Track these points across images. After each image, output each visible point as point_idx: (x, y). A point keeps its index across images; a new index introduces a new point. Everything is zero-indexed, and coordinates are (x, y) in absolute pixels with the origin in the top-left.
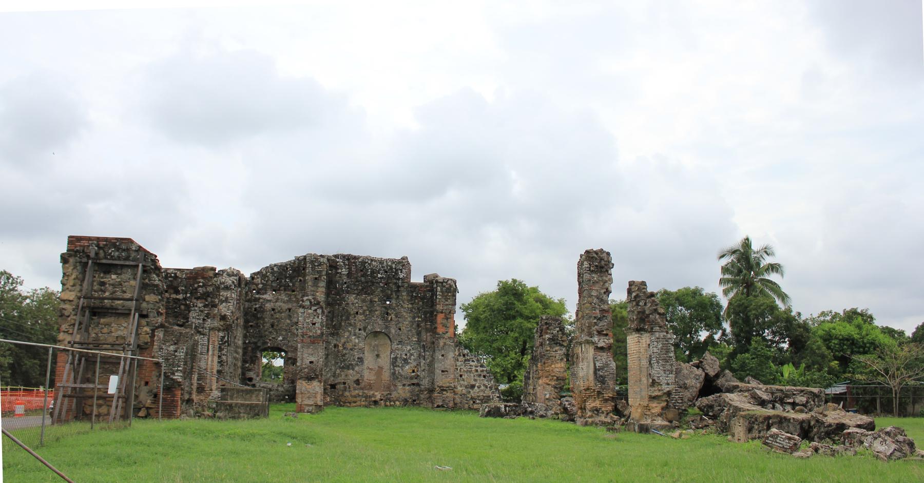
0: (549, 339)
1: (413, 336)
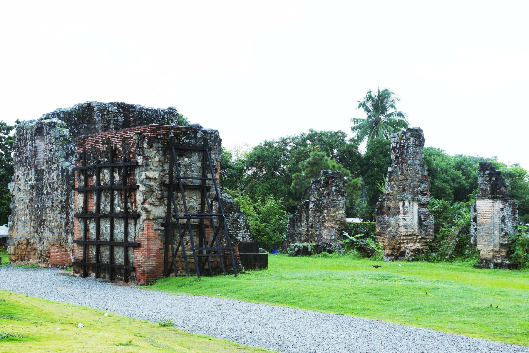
0: (336, 190)
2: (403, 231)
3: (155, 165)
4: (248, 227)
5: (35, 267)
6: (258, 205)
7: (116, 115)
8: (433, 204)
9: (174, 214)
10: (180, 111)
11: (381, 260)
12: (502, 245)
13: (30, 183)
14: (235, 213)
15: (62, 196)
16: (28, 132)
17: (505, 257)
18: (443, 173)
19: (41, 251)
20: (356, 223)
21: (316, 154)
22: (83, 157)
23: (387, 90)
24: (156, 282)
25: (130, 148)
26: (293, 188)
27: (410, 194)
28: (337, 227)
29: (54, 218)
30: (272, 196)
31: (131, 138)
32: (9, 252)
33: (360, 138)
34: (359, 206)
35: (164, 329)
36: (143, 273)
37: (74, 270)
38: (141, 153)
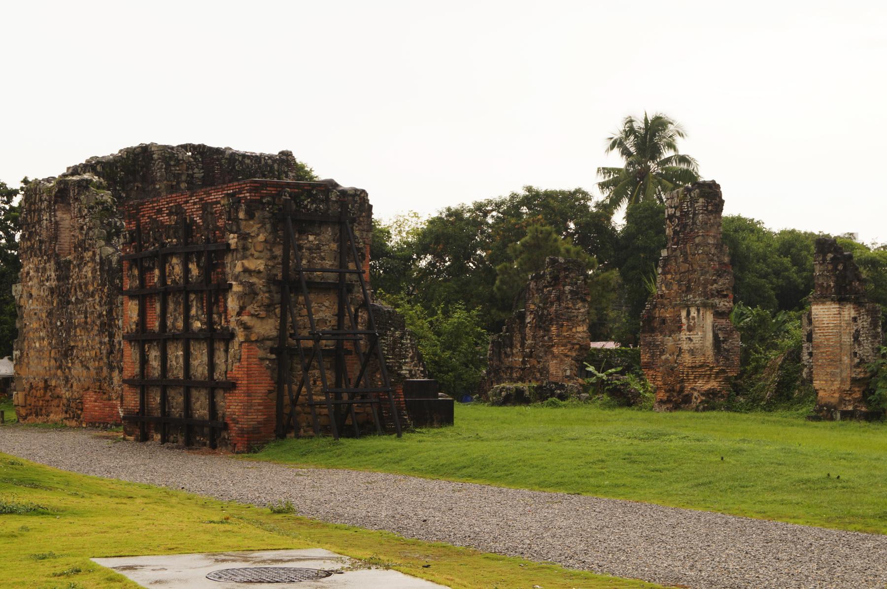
0: (571, 292)
2: (687, 359)
3: (259, 249)
4: (420, 358)
5: (60, 427)
6: (437, 320)
7: (190, 166)
8: (742, 314)
9: (292, 332)
10: (300, 158)
11: (651, 410)
12: (854, 381)
13: (47, 284)
14: (396, 329)
15: (101, 306)
16: (43, 198)
17: (860, 401)
18: (758, 261)
19: (68, 400)
20: (609, 350)
21: (537, 230)
22: (135, 237)
23: (661, 118)
24: (263, 447)
25: (216, 220)
26: (499, 289)
27: (700, 295)
28: (574, 354)
29: (89, 343)
30: (461, 304)
31: (218, 202)
32: (16, 403)
33: (615, 203)
34: (614, 321)
35: (279, 516)
36: (242, 432)
37: (125, 430)
38: (234, 228)
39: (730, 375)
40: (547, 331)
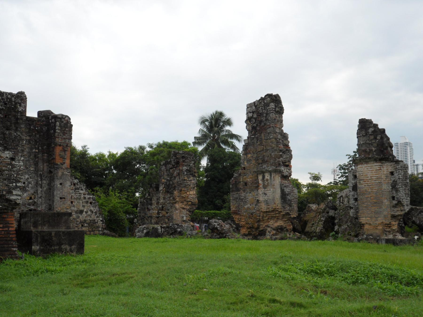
0: (187, 170)
1: (30, 166)
28: (188, 208)
39: (292, 216)
40: (172, 193)
